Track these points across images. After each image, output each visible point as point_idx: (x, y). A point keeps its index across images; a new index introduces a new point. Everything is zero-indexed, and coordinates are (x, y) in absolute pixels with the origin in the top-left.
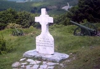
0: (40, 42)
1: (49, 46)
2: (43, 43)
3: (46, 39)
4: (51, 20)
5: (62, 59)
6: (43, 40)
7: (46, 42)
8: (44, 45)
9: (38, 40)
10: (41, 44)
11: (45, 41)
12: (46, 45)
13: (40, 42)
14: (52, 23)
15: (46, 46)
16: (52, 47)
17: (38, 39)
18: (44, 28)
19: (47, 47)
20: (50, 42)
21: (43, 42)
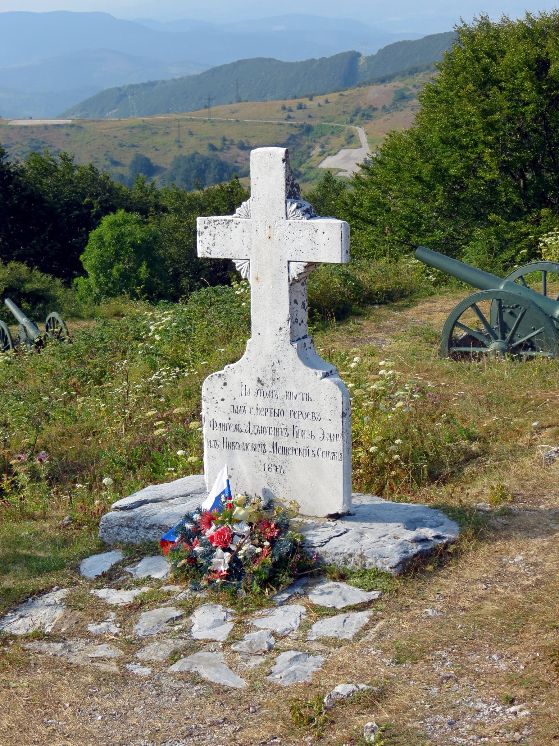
0: (237, 418)
1: (307, 452)
2: (261, 430)
3: (290, 395)
4: (326, 241)
5: (416, 549)
6: (262, 402)
7: (285, 421)
8: (267, 439)
9: (225, 406)
10: (246, 438)
11: (283, 413)
12: (284, 441)
13: (237, 418)
14: (204, 211)
15: (285, 450)
16: (213, 424)
17: (224, 394)
18: (270, 307)
19: (294, 458)
20: (315, 417)
21: (264, 421)
